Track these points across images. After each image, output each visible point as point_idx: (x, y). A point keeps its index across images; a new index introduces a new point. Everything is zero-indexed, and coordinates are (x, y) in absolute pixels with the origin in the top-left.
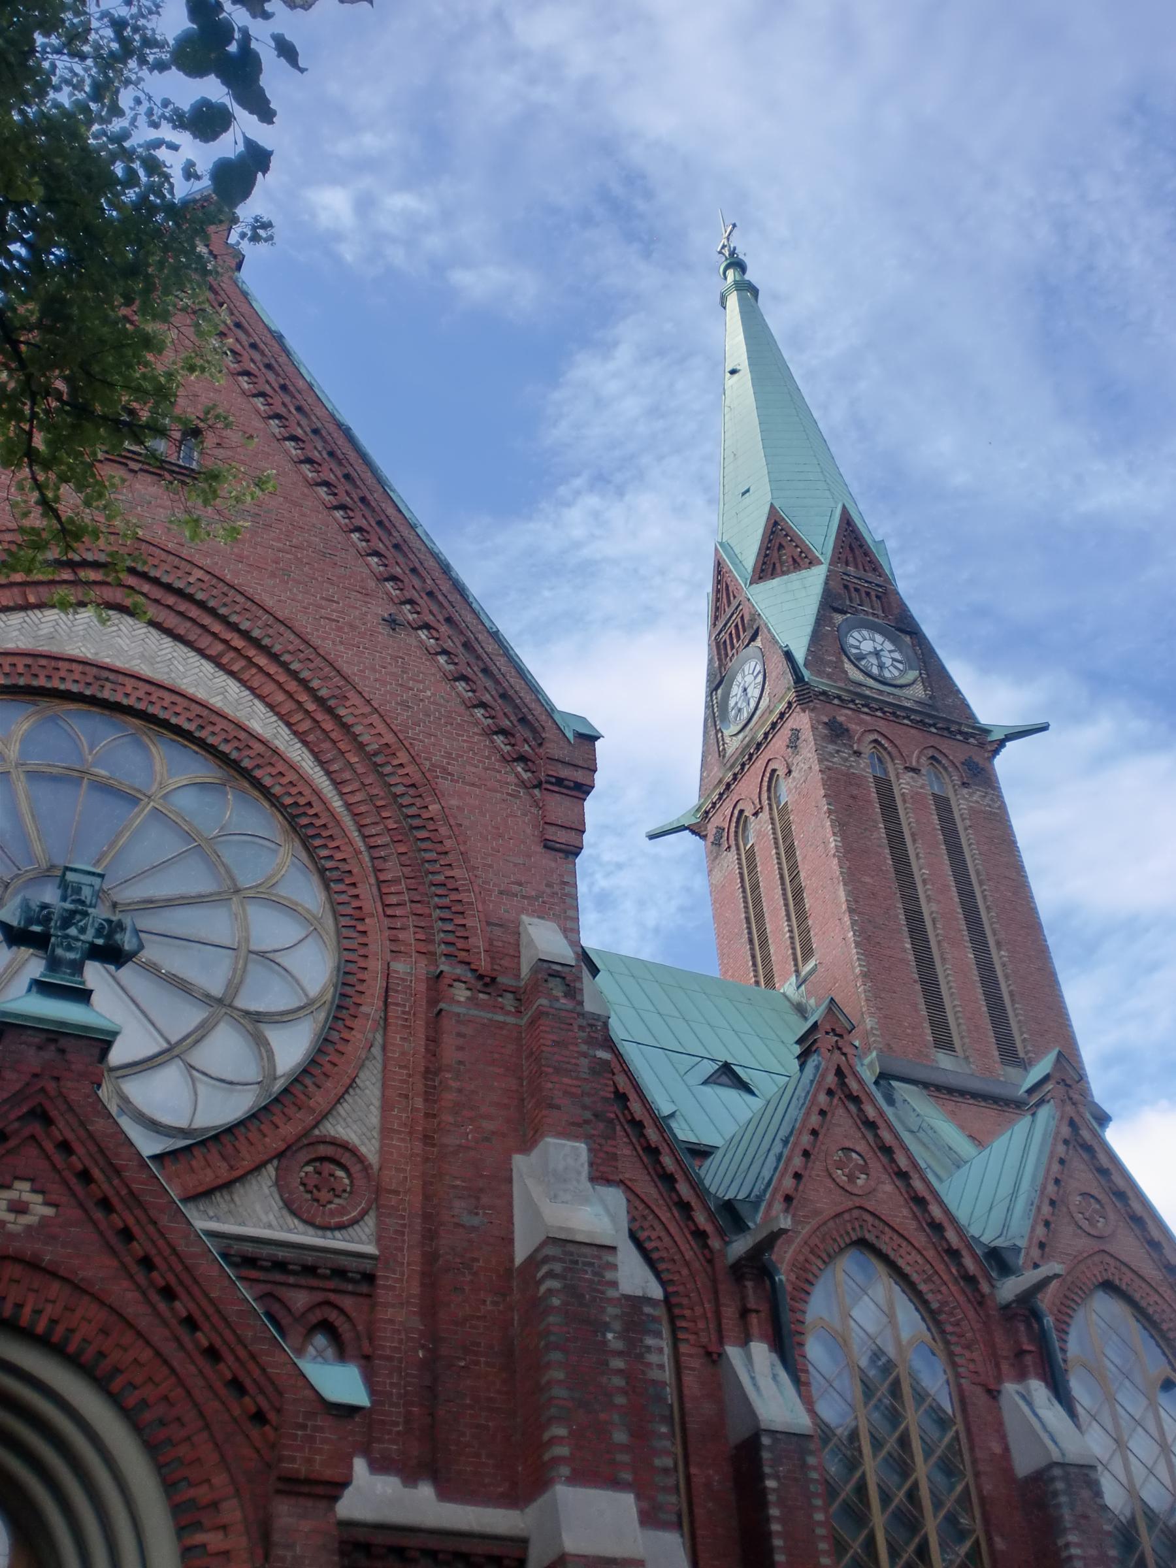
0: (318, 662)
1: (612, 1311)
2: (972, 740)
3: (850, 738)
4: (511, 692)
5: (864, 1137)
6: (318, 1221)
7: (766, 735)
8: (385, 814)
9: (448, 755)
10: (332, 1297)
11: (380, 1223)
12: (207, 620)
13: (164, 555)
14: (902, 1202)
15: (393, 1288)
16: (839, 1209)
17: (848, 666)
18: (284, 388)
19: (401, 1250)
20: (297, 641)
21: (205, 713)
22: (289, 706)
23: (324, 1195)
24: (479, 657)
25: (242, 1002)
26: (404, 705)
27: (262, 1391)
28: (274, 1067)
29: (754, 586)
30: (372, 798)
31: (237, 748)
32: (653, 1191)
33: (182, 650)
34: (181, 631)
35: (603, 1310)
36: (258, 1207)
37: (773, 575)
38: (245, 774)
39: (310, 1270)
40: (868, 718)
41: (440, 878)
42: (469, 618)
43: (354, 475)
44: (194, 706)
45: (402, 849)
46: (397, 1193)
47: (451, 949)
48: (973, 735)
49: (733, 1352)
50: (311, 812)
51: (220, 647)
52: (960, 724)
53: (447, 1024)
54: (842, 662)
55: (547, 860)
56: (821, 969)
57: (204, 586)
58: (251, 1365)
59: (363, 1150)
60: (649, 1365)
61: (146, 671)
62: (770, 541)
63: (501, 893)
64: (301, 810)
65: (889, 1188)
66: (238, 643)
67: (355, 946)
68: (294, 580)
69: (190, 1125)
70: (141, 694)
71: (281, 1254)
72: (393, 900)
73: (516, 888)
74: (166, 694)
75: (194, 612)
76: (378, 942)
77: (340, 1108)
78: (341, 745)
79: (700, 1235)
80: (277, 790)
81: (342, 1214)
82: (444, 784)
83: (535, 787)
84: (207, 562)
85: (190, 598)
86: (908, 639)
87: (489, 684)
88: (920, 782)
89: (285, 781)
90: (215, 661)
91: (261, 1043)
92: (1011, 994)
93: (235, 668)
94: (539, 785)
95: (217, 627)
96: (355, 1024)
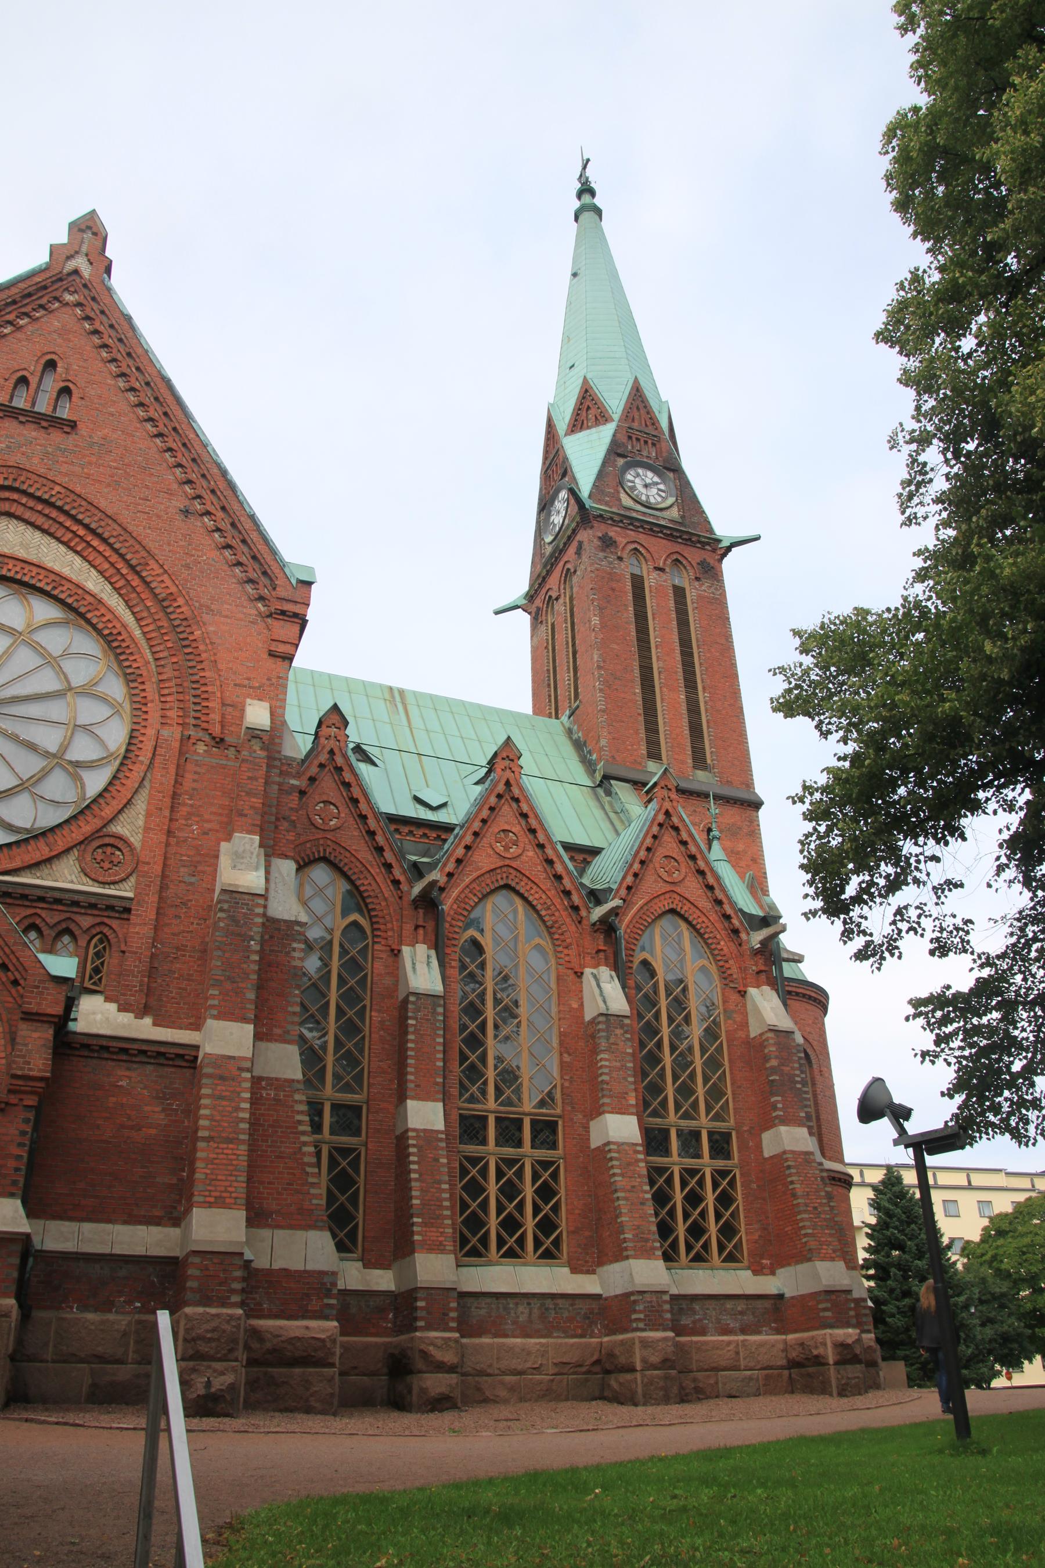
0: (131, 542)
1: (255, 929)
2: (708, 547)
3: (617, 547)
4: (258, 556)
7: (565, 544)
8: (166, 638)
10: (106, 920)
12: (62, 518)
13: (36, 478)
14: (539, 862)
15: (141, 916)
16: (493, 867)
17: (623, 495)
18: (129, 354)
19: (148, 895)
21: (57, 579)
23: (106, 865)
25: (68, 757)
26: (187, 567)
27: (17, 970)
28: (85, 794)
30: (160, 627)
31: (77, 601)
32: (370, 858)
33: (47, 539)
34: (46, 527)
35: (251, 929)
36: (66, 872)
37: (581, 429)
38: (82, 616)
40: (632, 533)
41: (196, 678)
43: (170, 413)
45: (175, 660)
46: (148, 863)
47: (198, 722)
48: (708, 544)
49: (406, 950)
50: (120, 638)
51: (70, 535)
52: (699, 536)
53: (190, 766)
54: (618, 492)
55: (270, 663)
56: (581, 707)
57: (61, 496)
58: (12, 956)
59: (132, 839)
60: (293, 958)
61: (22, 554)
62: (581, 404)
63: (236, 685)
64: (114, 637)
65: (531, 854)
66: (81, 532)
67: (140, 720)
69: (33, 824)
70: (18, 569)
71: (76, 898)
73: (246, 682)
75: (54, 514)
78: (143, 596)
79: (396, 883)
80: (100, 626)
82: (206, 617)
83: (268, 616)
84: (64, 480)
85: (52, 505)
86: (671, 475)
87: (246, 549)
89: (104, 619)
90: (66, 544)
91: (77, 779)
92: (708, 722)
93: (79, 549)
94: (270, 615)
95: (68, 523)
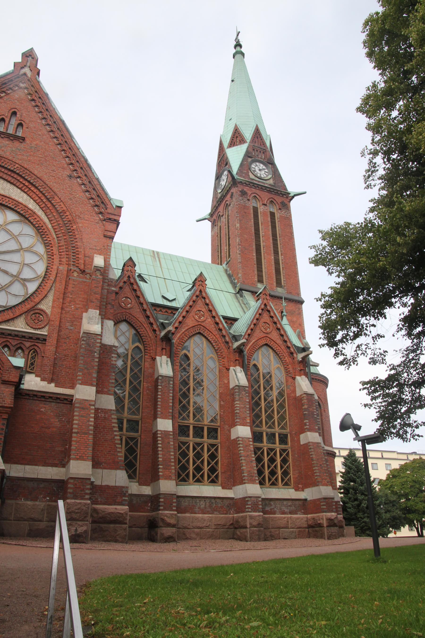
0: (48, 188)
2: (285, 196)
3: (247, 195)
4: (100, 195)
5: (205, 307)
6: (34, 327)
7: (226, 193)
8: (62, 229)
9: (81, 213)
10: (36, 344)
11: (49, 329)
12: (19, 178)
13: (8, 161)
16: (194, 325)
20: (42, 183)
21: (17, 203)
22: (39, 200)
23: (36, 321)
24: (92, 185)
29: (228, 149)
31: (25, 212)
32: (144, 320)
33: (12, 186)
34: (12, 181)
36: (20, 324)
37: (234, 145)
38: (27, 219)
39: (31, 338)
41: (74, 245)
42: (91, 175)
43: (64, 135)
44: (14, 201)
45: (65, 238)
47: (74, 263)
48: (285, 195)
49: (158, 358)
50: (43, 228)
51: (22, 185)
52: (281, 191)
53: (71, 282)
55: (104, 240)
57: (19, 169)
60: (112, 360)
62: (234, 135)
65: (209, 320)
66: (27, 184)
68: (44, 166)
71: (24, 334)
72: (61, 251)
73: (95, 247)
74: (7, 199)
75: (16, 176)
76: (56, 261)
77: (42, 302)
78: (52, 211)
79: (154, 331)
80: (34, 223)
81: (40, 326)
82: (79, 220)
83: (103, 220)
85: (15, 172)
86: (270, 166)
87: (95, 193)
88: (266, 208)
89: (36, 220)
90: (20, 189)
91: (24, 286)
92: (283, 268)
93: (26, 191)
94: (105, 220)
96: (48, 282)
